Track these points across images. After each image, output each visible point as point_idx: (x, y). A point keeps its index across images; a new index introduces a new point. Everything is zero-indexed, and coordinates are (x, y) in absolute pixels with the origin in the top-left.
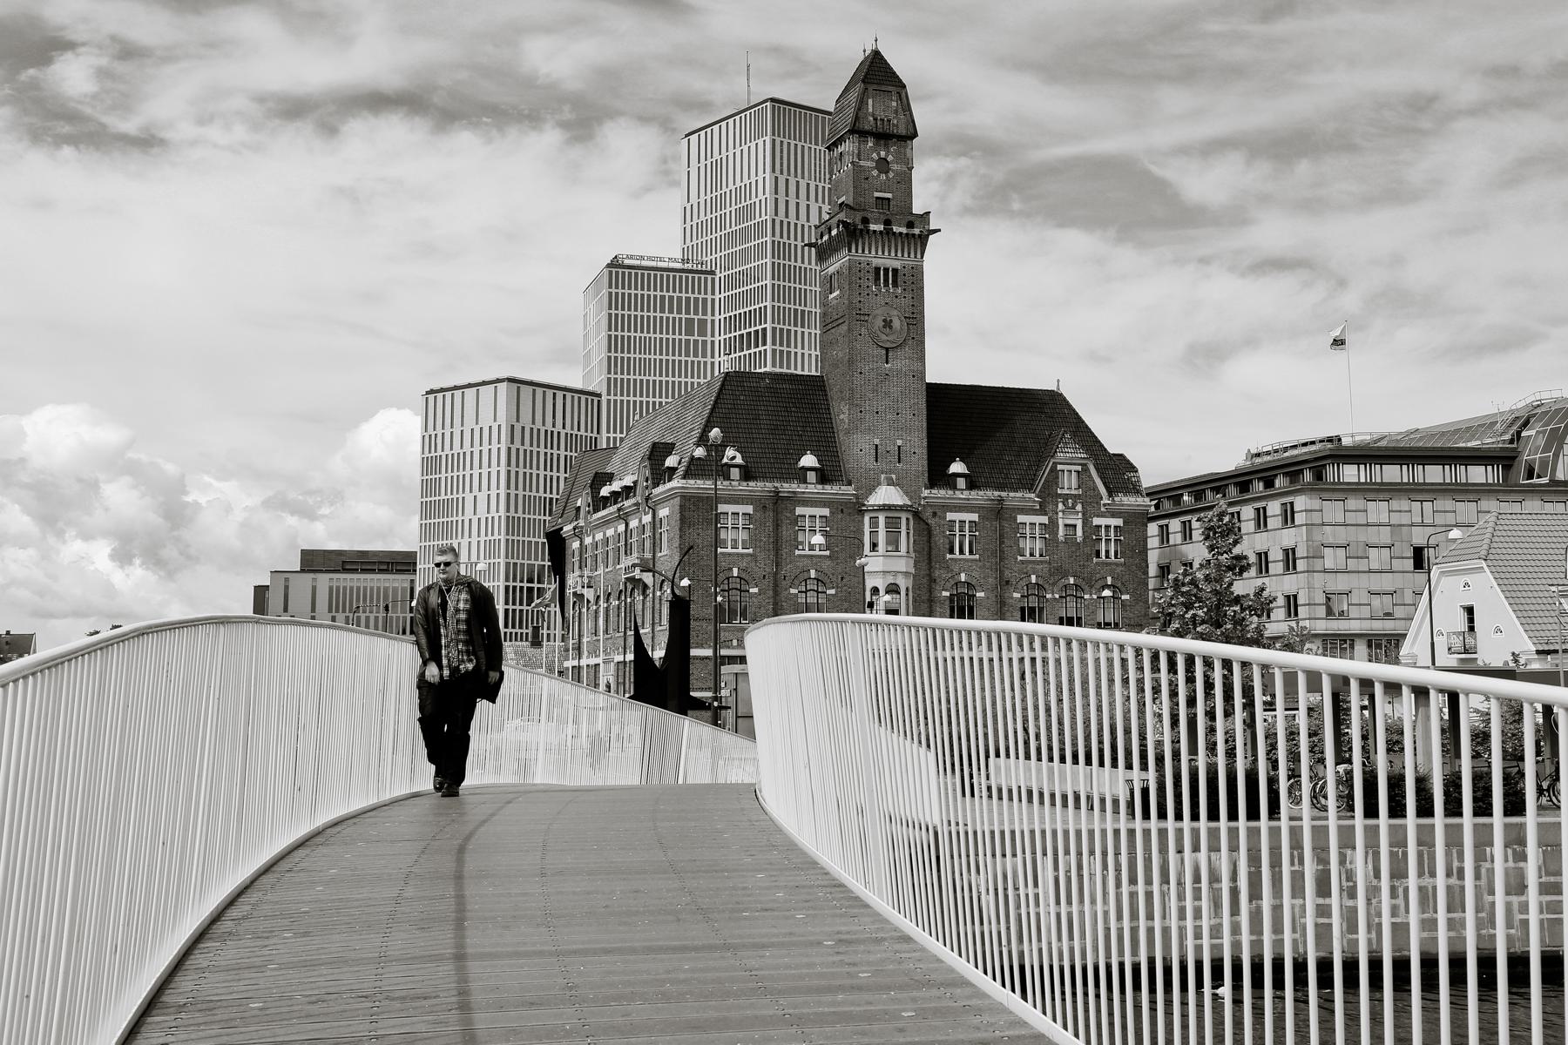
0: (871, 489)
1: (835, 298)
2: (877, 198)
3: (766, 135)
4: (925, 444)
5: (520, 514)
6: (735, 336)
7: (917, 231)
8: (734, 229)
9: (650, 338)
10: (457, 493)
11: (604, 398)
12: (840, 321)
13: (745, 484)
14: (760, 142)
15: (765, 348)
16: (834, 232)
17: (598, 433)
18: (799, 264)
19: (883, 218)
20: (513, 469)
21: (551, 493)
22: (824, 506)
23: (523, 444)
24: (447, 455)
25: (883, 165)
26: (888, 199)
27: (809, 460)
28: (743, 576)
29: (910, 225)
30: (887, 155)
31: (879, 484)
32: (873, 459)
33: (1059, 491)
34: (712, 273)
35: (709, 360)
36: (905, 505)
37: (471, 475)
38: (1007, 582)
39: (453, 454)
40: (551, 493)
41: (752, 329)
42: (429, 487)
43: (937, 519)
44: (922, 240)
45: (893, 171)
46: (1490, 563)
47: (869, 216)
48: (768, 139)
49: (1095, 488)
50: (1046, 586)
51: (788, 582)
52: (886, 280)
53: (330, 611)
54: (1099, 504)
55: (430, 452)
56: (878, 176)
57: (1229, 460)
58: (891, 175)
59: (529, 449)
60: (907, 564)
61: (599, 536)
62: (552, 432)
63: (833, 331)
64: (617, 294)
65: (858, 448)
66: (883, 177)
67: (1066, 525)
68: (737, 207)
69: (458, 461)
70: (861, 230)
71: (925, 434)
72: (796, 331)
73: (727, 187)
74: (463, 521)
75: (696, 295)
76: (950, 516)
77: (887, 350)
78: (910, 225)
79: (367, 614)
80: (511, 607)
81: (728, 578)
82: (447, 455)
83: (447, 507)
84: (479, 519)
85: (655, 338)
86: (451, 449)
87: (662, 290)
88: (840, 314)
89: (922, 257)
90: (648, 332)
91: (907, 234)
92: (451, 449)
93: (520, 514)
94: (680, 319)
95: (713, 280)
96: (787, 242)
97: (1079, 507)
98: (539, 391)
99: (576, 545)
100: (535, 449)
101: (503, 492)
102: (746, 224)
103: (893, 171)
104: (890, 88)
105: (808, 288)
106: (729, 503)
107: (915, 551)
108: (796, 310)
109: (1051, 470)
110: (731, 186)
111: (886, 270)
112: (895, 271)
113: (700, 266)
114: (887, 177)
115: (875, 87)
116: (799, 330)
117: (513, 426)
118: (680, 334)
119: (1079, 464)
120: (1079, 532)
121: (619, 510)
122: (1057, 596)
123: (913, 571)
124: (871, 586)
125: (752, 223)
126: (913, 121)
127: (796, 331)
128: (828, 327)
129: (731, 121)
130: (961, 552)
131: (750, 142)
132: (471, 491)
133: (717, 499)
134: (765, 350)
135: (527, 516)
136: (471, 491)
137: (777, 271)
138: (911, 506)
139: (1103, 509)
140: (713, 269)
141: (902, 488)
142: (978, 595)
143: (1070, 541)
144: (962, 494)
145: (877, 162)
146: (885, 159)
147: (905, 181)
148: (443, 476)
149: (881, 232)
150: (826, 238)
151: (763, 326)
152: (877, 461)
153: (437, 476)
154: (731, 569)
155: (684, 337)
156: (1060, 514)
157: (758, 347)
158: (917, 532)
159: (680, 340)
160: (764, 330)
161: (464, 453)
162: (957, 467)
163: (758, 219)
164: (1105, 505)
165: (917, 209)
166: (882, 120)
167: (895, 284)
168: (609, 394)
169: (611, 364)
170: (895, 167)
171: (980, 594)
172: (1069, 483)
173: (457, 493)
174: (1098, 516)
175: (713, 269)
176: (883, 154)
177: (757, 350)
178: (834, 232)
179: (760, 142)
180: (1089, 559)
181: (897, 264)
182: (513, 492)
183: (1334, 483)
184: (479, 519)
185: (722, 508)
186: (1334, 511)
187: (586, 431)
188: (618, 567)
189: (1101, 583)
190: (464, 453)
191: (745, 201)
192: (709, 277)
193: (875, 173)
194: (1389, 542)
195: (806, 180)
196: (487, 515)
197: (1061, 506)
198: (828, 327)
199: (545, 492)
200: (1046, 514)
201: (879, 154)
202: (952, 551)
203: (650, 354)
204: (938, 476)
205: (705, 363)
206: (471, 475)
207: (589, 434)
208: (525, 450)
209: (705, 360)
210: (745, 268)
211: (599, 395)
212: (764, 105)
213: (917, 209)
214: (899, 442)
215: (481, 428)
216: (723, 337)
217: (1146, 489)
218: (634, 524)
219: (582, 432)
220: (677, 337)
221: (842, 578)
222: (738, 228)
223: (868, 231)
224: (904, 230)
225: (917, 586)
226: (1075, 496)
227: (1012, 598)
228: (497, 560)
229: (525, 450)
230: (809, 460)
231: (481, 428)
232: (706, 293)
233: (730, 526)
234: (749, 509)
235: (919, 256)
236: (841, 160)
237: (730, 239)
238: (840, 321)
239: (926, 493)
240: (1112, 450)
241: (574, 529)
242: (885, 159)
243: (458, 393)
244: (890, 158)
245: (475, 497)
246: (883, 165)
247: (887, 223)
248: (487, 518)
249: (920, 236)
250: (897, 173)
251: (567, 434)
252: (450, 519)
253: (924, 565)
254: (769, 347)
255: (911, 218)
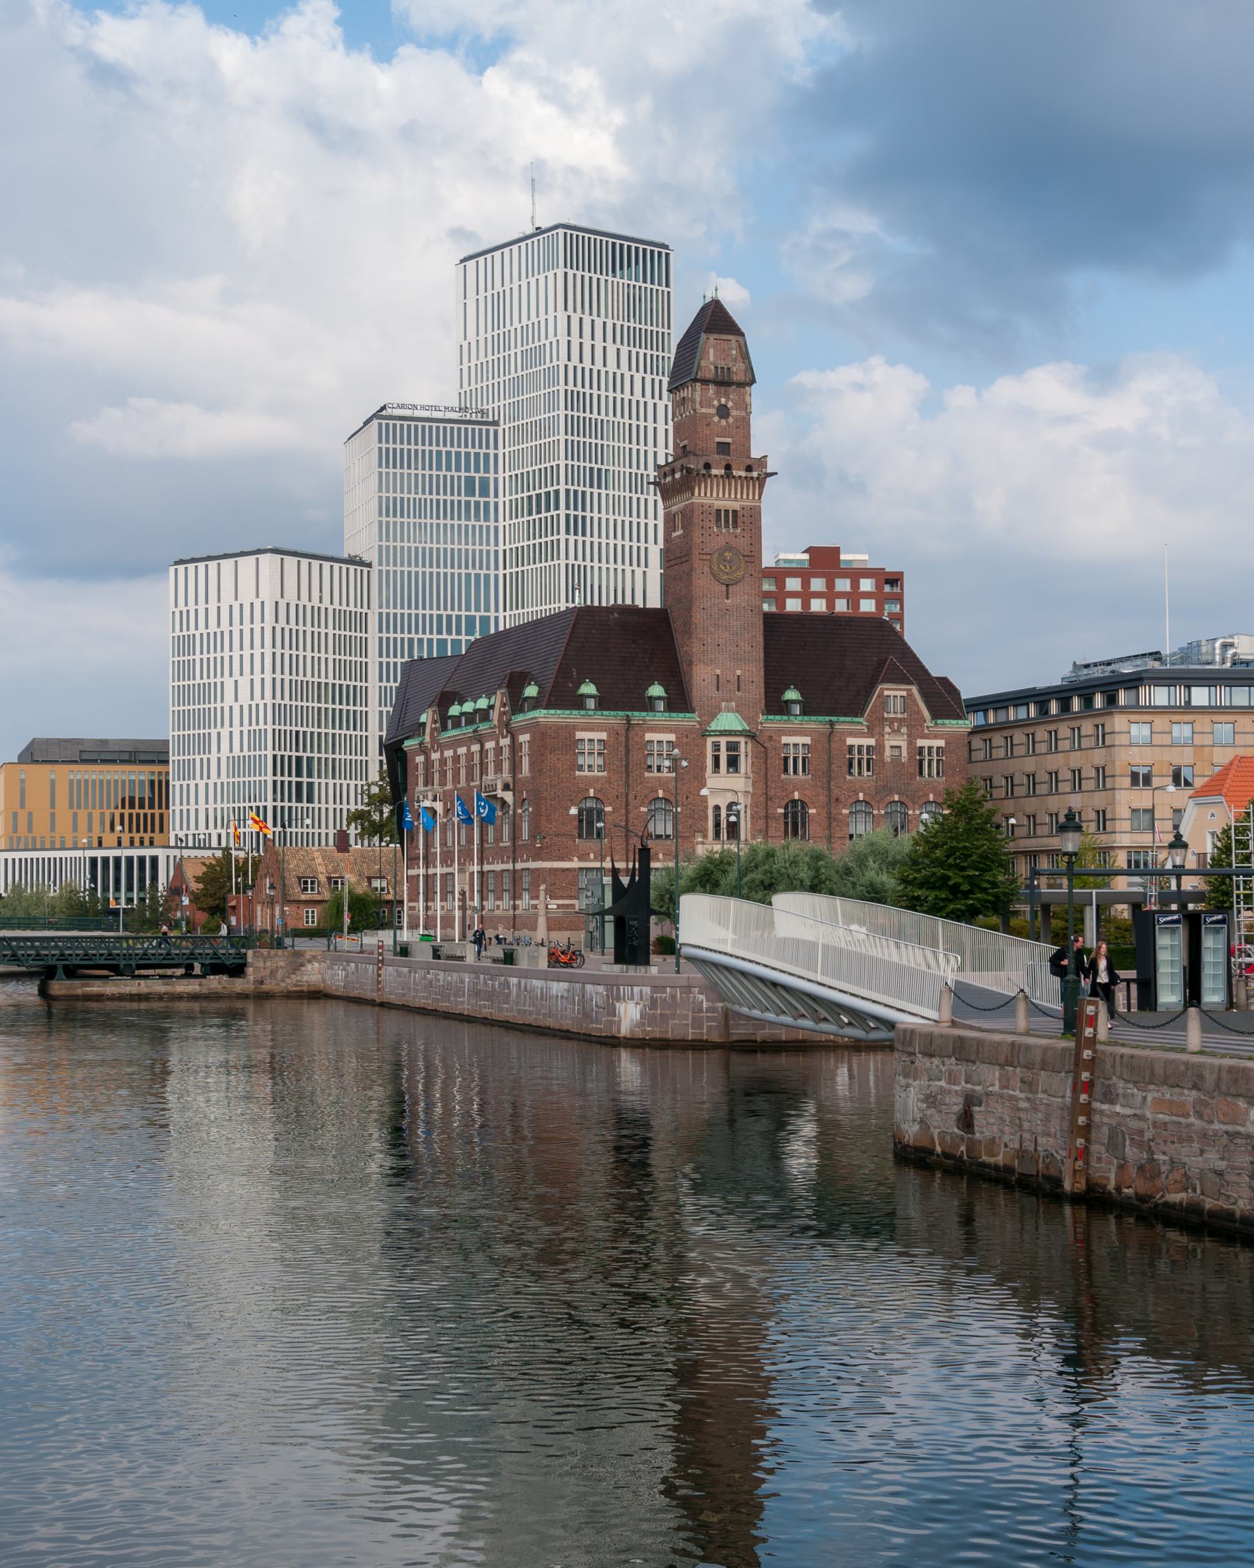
0: (713, 716)
1: (679, 537)
2: (718, 443)
3: (558, 267)
4: (762, 673)
5: (287, 701)
6: (522, 498)
7: (755, 474)
8: (519, 373)
9: (426, 500)
10: (215, 676)
11: (376, 568)
12: (684, 560)
13: (599, 713)
14: (550, 275)
15: (557, 512)
16: (678, 475)
17: (369, 608)
18: (595, 415)
19: (724, 463)
20: (279, 651)
21: (319, 677)
22: (671, 732)
23: (288, 623)
24: (202, 634)
25: (723, 412)
26: (729, 443)
27: (656, 690)
28: (599, 796)
29: (749, 469)
30: (727, 402)
31: (720, 711)
32: (714, 688)
33: (886, 715)
34: (495, 423)
35: (492, 524)
36: (744, 730)
37: (231, 657)
38: (837, 800)
39: (208, 634)
40: (319, 677)
41: (543, 491)
42: (184, 670)
43: (773, 743)
44: (761, 481)
45: (733, 417)
46: (1228, 799)
47: (710, 460)
48: (560, 272)
49: (919, 712)
50: (873, 803)
51: (639, 800)
52: (727, 521)
53: (71, 806)
54: (922, 726)
55: (181, 630)
56: (719, 422)
57: (1052, 675)
58: (731, 420)
59: (294, 628)
60: (746, 784)
61: (449, 753)
62: (319, 608)
63: (676, 567)
64: (387, 449)
65: (702, 677)
66: (724, 422)
67: (892, 747)
68: (524, 349)
69: (215, 641)
70: (704, 475)
71: (762, 664)
72: (592, 493)
73: (511, 325)
74: (222, 708)
75: (477, 450)
76: (785, 740)
77: (727, 585)
78: (749, 469)
79: (113, 811)
80: (279, 804)
81: (585, 798)
82: (202, 634)
83: (205, 693)
84: (241, 706)
85: (431, 500)
86: (207, 627)
87: (438, 445)
88: (684, 553)
89: (760, 498)
90: (424, 493)
91: (746, 477)
92: (207, 627)
93: (287, 701)
94: (459, 477)
95: (496, 432)
96: (582, 390)
97: (904, 730)
98: (305, 562)
99: (420, 759)
100: (301, 628)
101: (268, 676)
102: (534, 370)
103: (733, 417)
104: (730, 337)
105: (605, 442)
106: (586, 730)
107: (753, 772)
108: (592, 469)
109: (879, 696)
110: (516, 324)
111: (727, 511)
112: (735, 512)
113: (479, 415)
114: (727, 422)
115: (716, 336)
116: (596, 491)
117: (277, 603)
118: (459, 494)
119: (904, 690)
120: (904, 753)
121: (475, 731)
122: (883, 812)
123: (751, 789)
124: (713, 804)
125: (542, 368)
126: (752, 369)
127: (592, 493)
128: (672, 563)
129: (515, 248)
130: (795, 772)
131: (539, 273)
132: (231, 675)
133: (573, 728)
134: (558, 515)
135: (294, 703)
136: (231, 675)
137: (572, 425)
138: (749, 731)
139: (926, 731)
140: (496, 419)
141: (741, 714)
142: (810, 811)
143: (896, 760)
144: (797, 721)
145: (718, 409)
146: (725, 406)
147: (744, 425)
148: (198, 657)
149: (722, 476)
150: (669, 479)
151: (556, 487)
152: (718, 690)
153: (191, 658)
154: (587, 790)
155: (463, 498)
156: (887, 737)
157: (537, 495)
158: (756, 756)
159: (459, 502)
160: (557, 492)
161: (222, 632)
162: (792, 695)
163: (548, 364)
164: (928, 727)
165: (755, 454)
166: (722, 368)
167: (735, 525)
168: (380, 564)
169: (384, 531)
170: (734, 413)
171: (812, 811)
172: (895, 711)
173: (215, 676)
174: (922, 738)
175: (496, 419)
176: (723, 401)
177: (548, 514)
178: (678, 475)
179: (550, 275)
180: (912, 777)
181: (736, 506)
182: (278, 676)
183: (1145, 707)
184: (241, 706)
185: (579, 735)
186: (1140, 731)
187: (356, 606)
188: (472, 784)
189: (923, 800)
190: (222, 632)
191: (533, 342)
192: (492, 429)
193: (716, 419)
194: (1191, 761)
195: (603, 319)
196: (251, 702)
197: (887, 729)
198: (672, 563)
199: (313, 676)
200: (873, 737)
201: (719, 401)
202: (786, 770)
203: (425, 518)
204: (776, 706)
205: (488, 527)
206: (231, 657)
207: (359, 610)
208: (291, 630)
209: (488, 524)
210: (533, 419)
211: (369, 565)
212: (554, 232)
213: (755, 454)
214: (739, 672)
215: (241, 605)
216: (508, 498)
217: (965, 700)
218: (490, 745)
219: (352, 608)
220: (456, 498)
221: (687, 798)
222: (524, 373)
223: (710, 476)
224: (743, 474)
225: (755, 805)
226: (900, 719)
227: (841, 814)
228: (263, 753)
229: (291, 630)
230: (656, 690)
231: (241, 605)
232: (488, 447)
233: (586, 751)
234: (604, 736)
235: (757, 497)
236: (683, 404)
237: (517, 385)
238: (684, 560)
239: (761, 718)
240: (935, 672)
241: (420, 744)
242: (725, 406)
243: (213, 565)
244: (730, 404)
245: (236, 681)
246: (723, 412)
247: (728, 467)
248: (250, 706)
249: (758, 478)
250: (736, 420)
251: (334, 610)
252: (207, 706)
253: (761, 785)
254: (562, 512)
255: (749, 462)
